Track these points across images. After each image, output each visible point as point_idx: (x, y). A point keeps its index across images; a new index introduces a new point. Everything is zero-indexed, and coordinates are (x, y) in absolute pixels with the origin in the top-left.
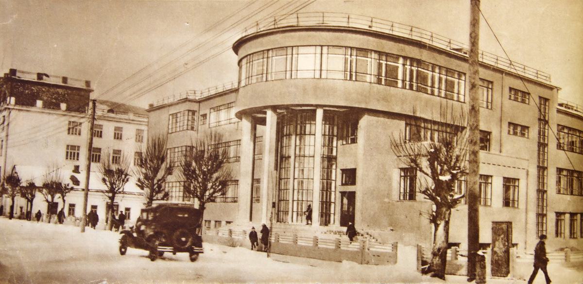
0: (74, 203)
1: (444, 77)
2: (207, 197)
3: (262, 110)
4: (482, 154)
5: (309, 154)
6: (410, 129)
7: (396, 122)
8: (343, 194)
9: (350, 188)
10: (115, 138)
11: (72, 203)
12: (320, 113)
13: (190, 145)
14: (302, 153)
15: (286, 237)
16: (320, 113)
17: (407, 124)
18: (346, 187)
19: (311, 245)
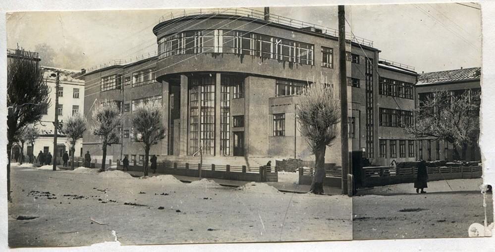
0: (48, 146)
1: (299, 48)
2: (86, 120)
3: (178, 75)
4: (200, 163)
5: (200, 165)
6: (279, 87)
7: (273, 80)
8: (235, 133)
9: (241, 129)
10: (74, 97)
11: (46, 146)
12: (218, 76)
13: (203, 164)
14: (206, 105)
15: (285, 19)
16: (218, 76)
17: (277, 84)
18: (236, 128)
19: (211, 170)
